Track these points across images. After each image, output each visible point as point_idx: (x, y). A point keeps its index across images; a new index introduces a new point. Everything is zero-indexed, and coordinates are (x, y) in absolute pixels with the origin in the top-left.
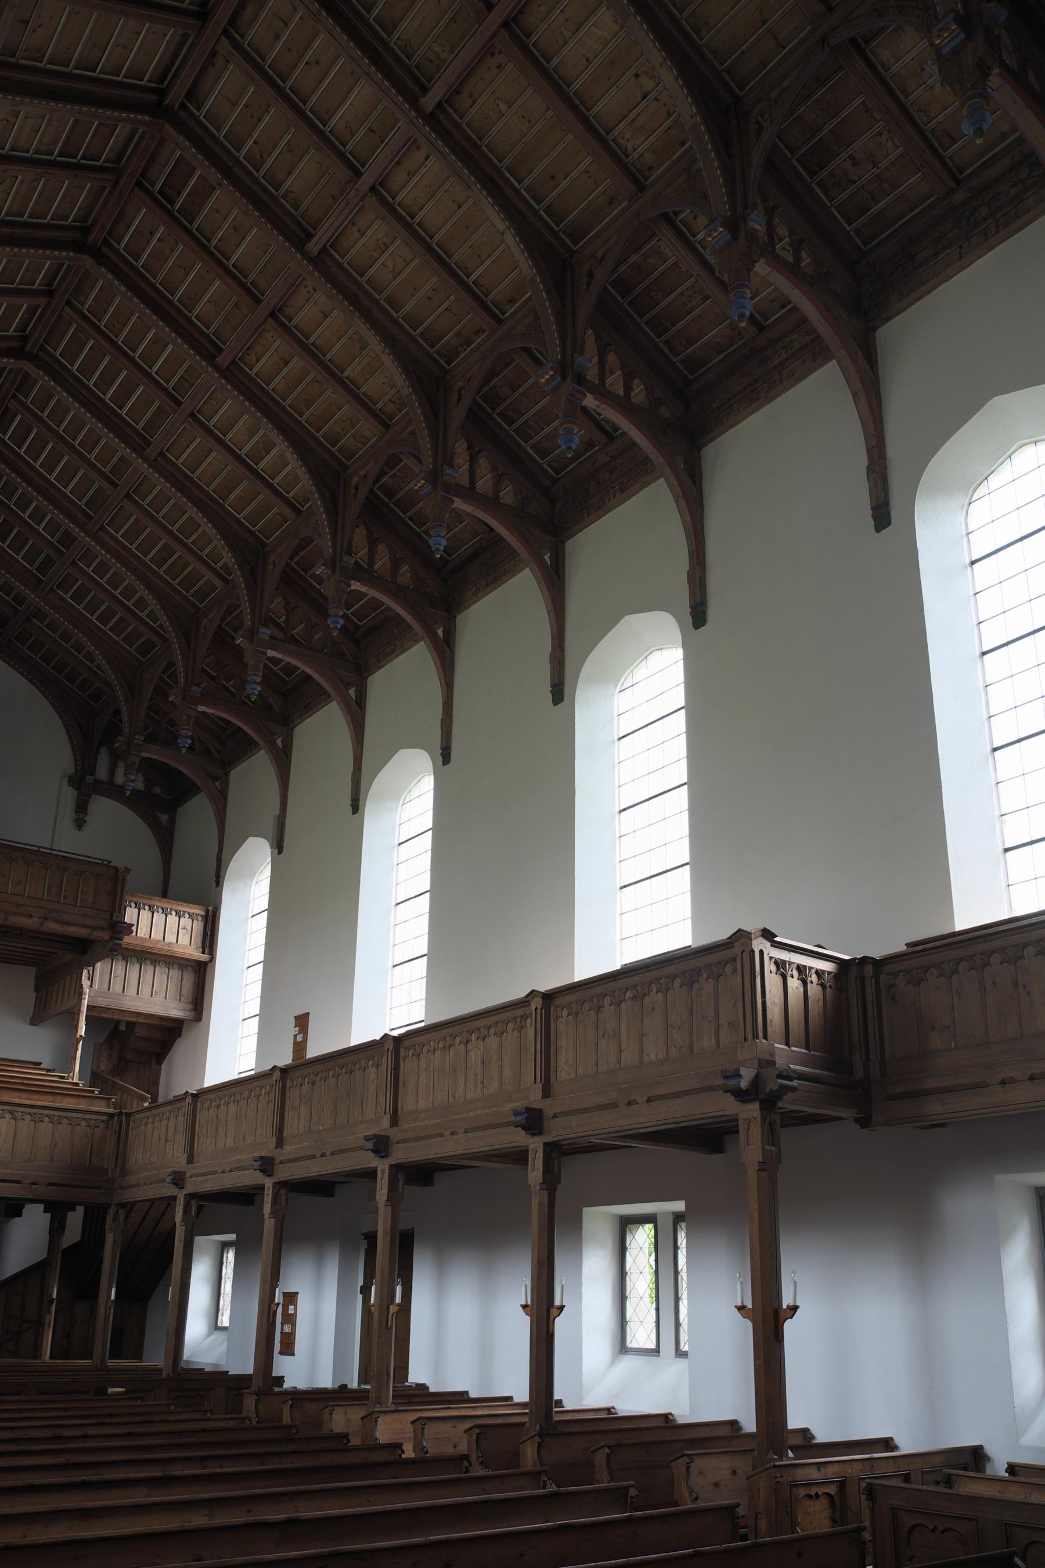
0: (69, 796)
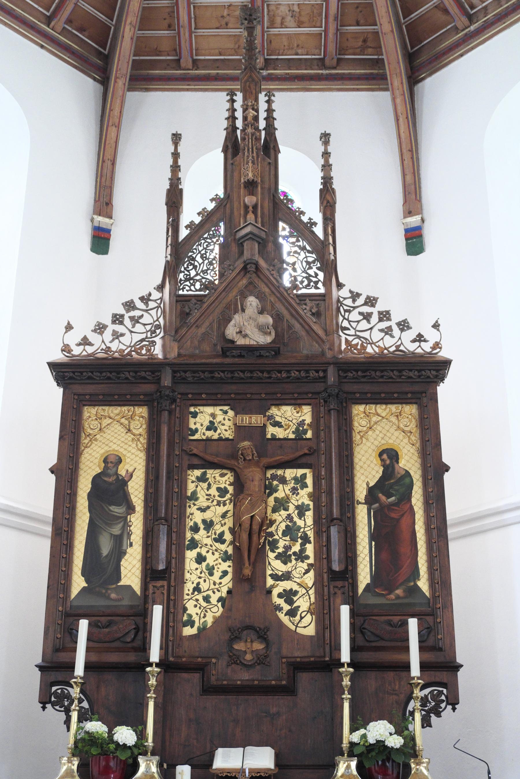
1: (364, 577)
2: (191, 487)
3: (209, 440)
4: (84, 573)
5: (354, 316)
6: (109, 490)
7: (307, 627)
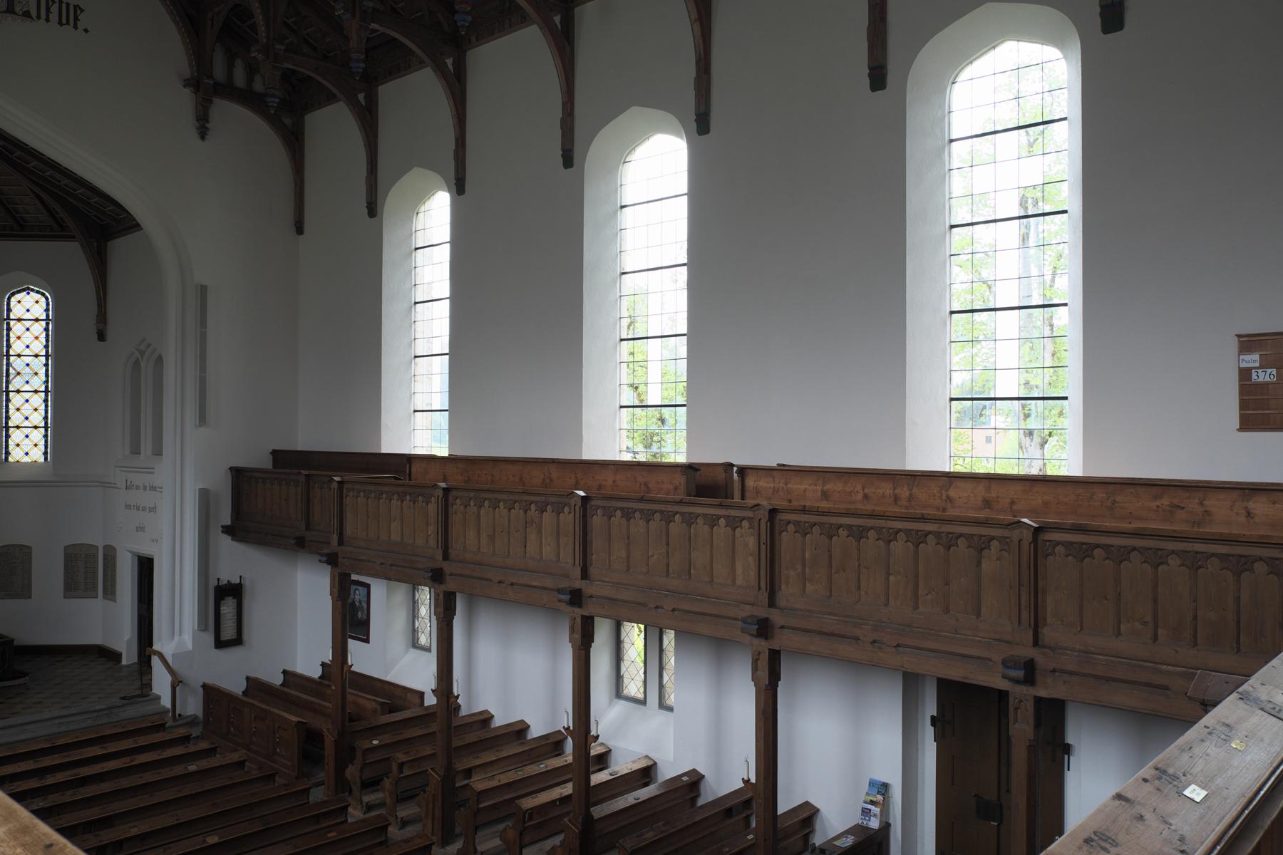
0: (185, 100)
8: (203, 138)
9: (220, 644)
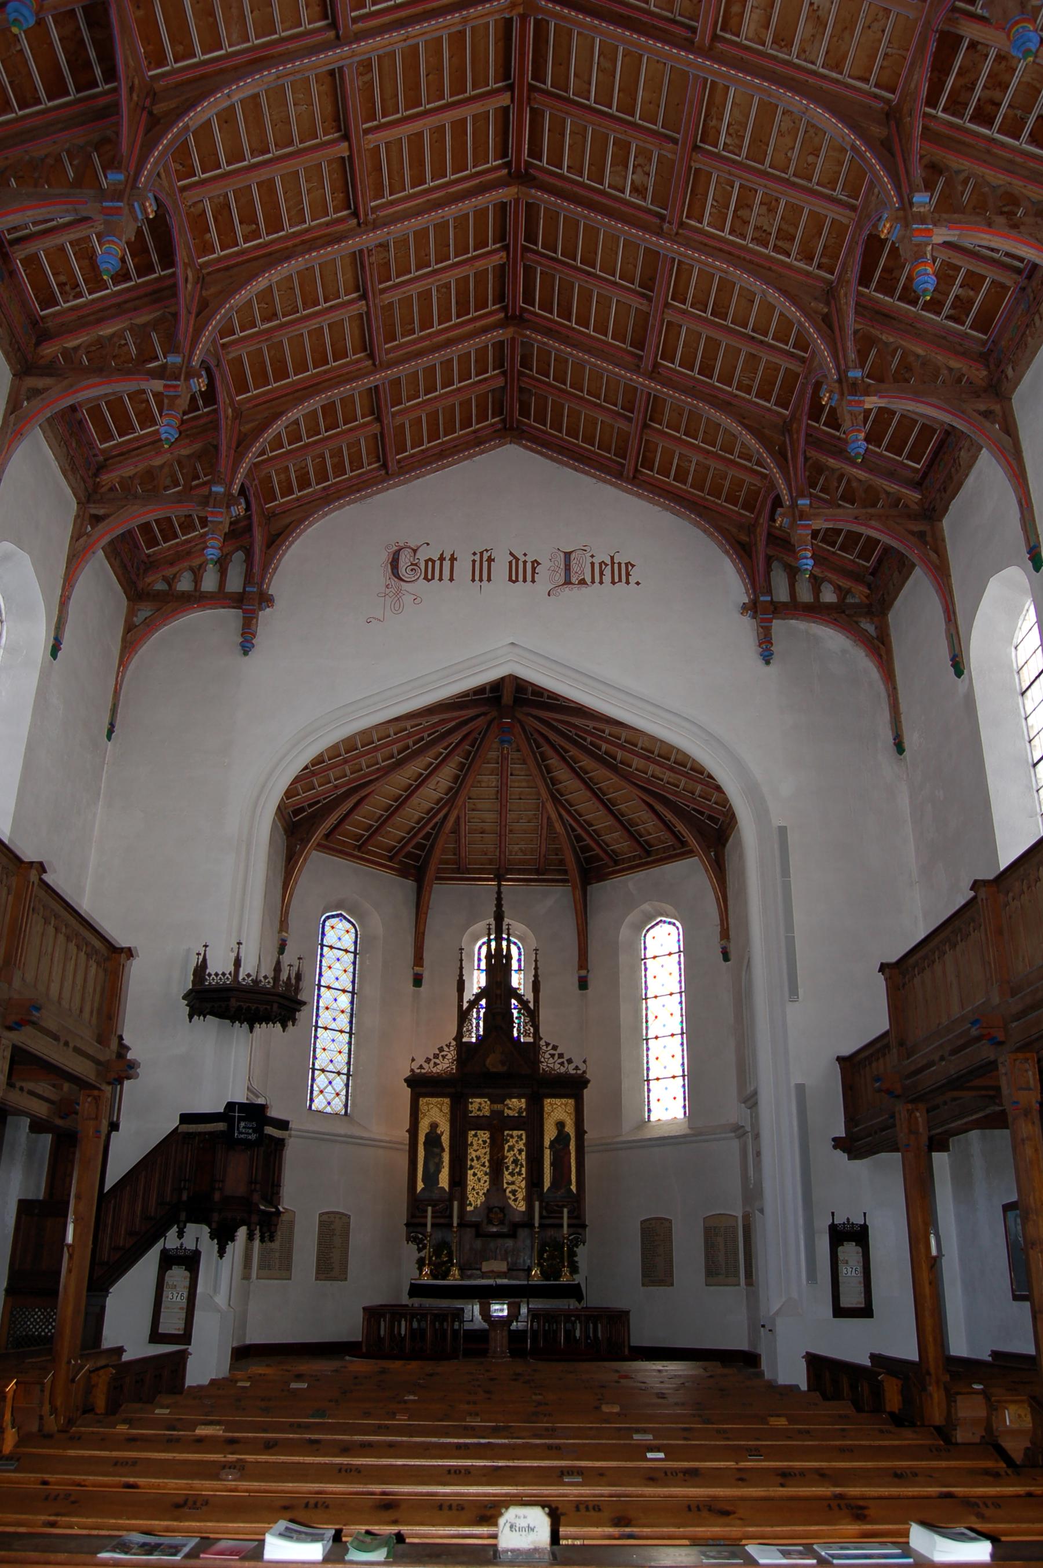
0: (746, 628)
1: (547, 1184)
2: (470, 1140)
3: (478, 1116)
4: (423, 1180)
5: (547, 1056)
6: (433, 1140)
7: (522, 1207)
8: (768, 663)
9: (839, 1312)
